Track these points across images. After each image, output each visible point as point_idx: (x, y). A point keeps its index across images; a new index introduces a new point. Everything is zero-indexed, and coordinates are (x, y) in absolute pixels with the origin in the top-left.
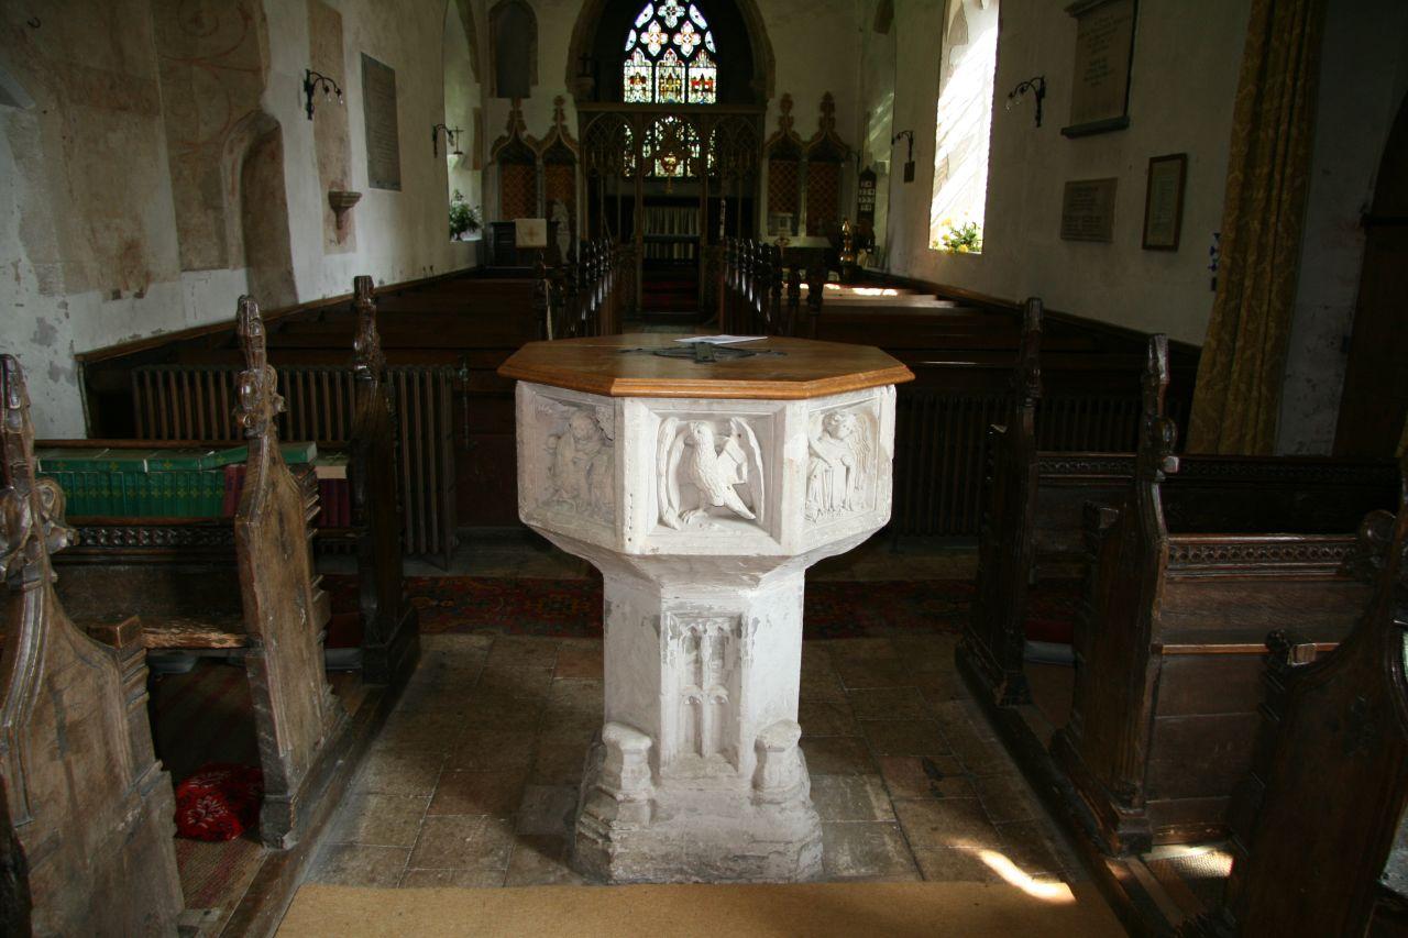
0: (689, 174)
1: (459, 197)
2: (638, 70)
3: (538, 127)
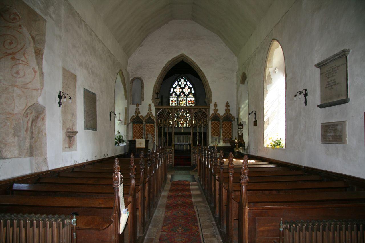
0: (188, 126)
1: (119, 133)
2: (174, 98)
3: (144, 113)
